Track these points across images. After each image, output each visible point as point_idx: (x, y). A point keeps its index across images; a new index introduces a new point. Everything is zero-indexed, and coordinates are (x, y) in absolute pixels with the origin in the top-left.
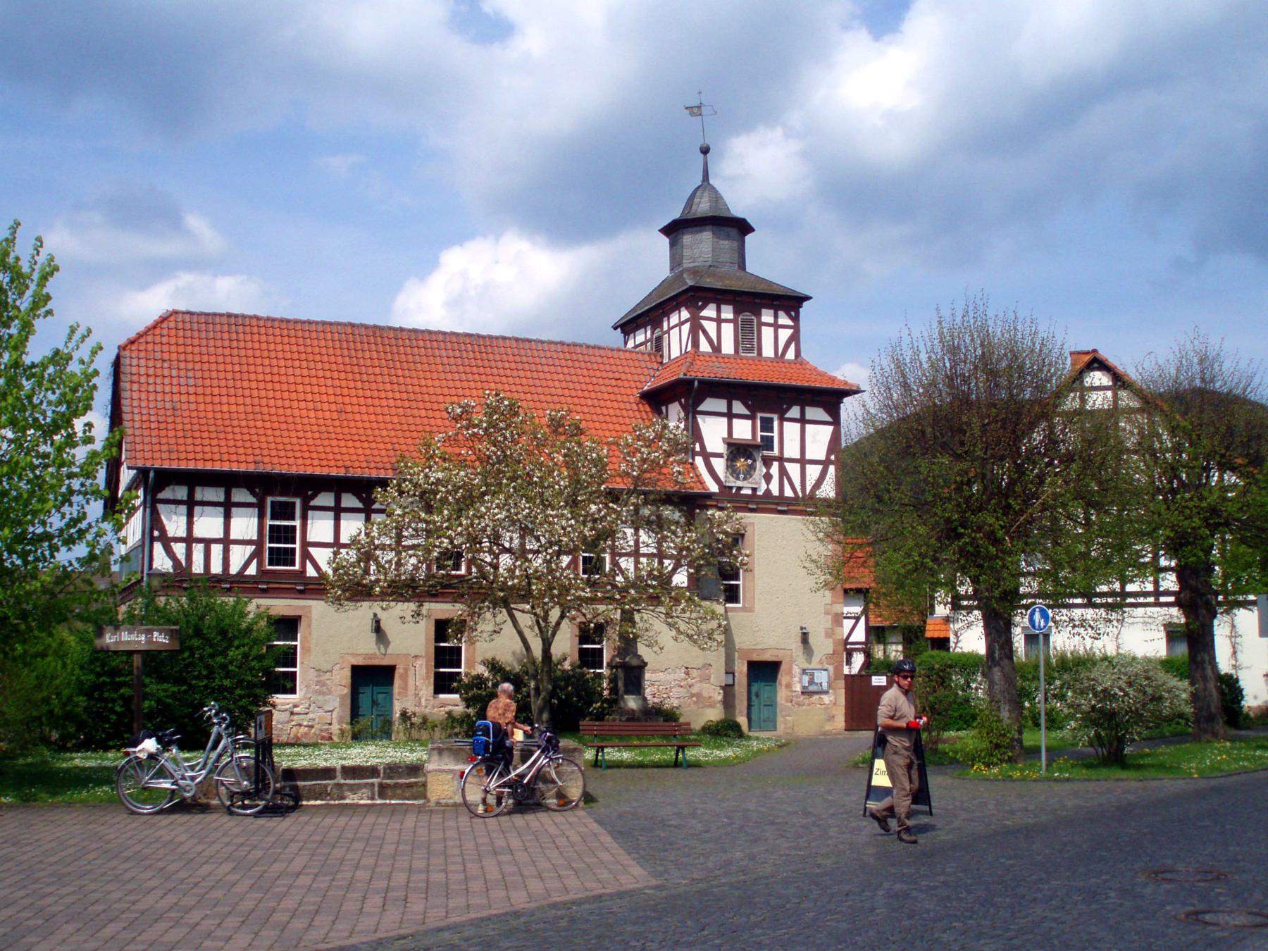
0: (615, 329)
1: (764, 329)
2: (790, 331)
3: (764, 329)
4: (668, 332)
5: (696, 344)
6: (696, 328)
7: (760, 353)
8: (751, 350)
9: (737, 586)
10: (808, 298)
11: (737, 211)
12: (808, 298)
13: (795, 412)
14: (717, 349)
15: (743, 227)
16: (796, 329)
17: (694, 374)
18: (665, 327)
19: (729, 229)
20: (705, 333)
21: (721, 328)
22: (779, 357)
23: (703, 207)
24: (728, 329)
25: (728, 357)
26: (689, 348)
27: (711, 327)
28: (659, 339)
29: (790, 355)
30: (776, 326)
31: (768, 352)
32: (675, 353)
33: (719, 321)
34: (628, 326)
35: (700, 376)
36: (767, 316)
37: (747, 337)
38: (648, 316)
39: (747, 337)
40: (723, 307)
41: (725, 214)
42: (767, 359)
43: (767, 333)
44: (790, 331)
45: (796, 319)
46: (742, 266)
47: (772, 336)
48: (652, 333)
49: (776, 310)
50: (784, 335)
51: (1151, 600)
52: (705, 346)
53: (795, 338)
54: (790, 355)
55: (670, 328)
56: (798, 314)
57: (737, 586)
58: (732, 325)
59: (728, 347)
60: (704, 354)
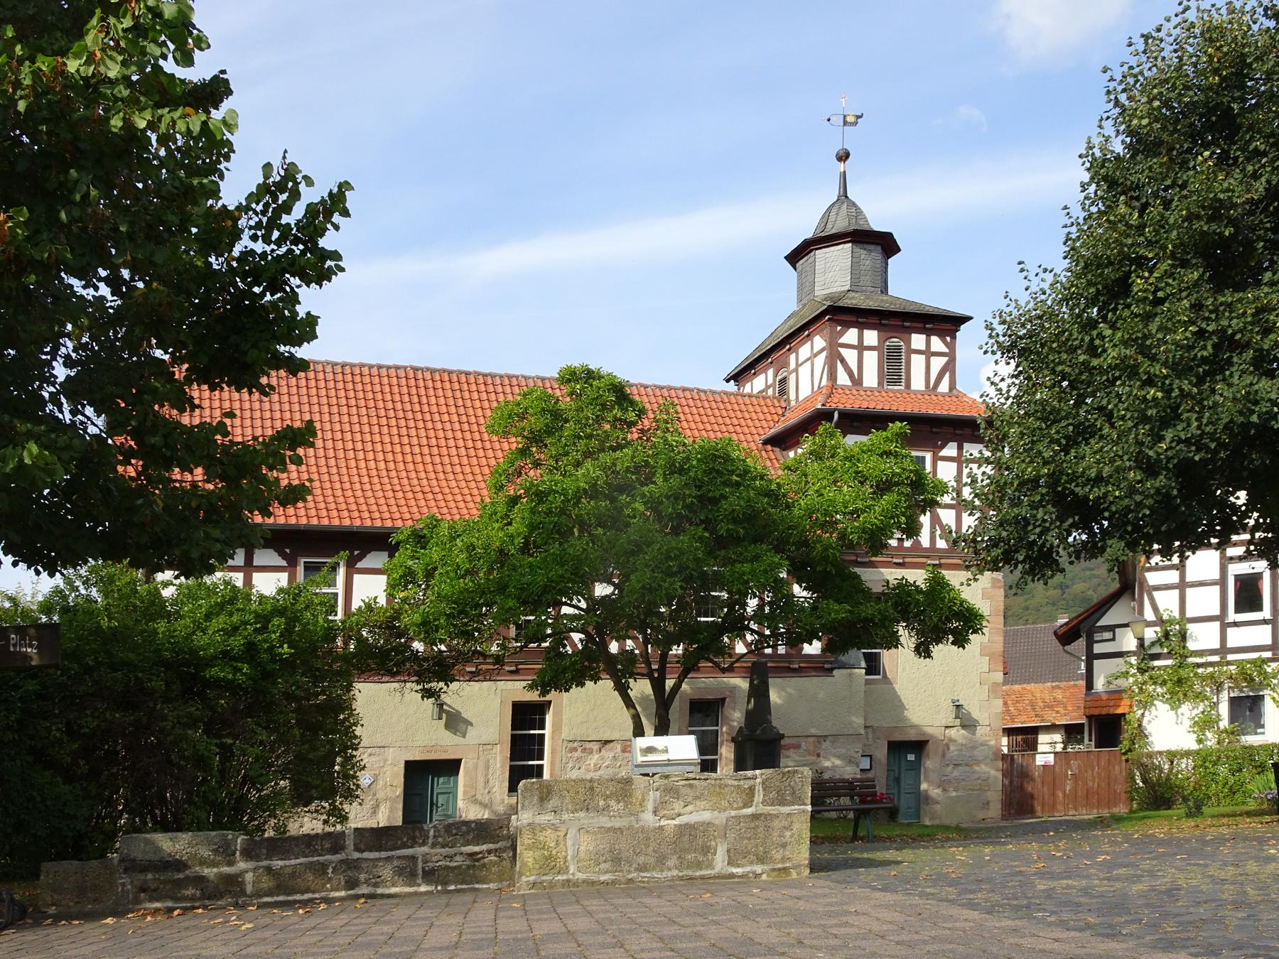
0: (728, 381)
1: (914, 356)
2: (944, 360)
3: (914, 356)
4: (796, 370)
5: (833, 376)
6: (834, 357)
7: (908, 386)
8: (897, 382)
9: (543, 735)
10: (971, 318)
11: (877, 226)
12: (971, 318)
13: (950, 450)
14: (857, 381)
15: (886, 245)
16: (951, 356)
17: (834, 406)
18: (793, 365)
19: (872, 247)
20: (843, 361)
21: (863, 352)
22: (932, 389)
23: (840, 224)
24: (871, 359)
25: (872, 390)
26: (824, 382)
27: (850, 356)
28: (784, 381)
29: (944, 387)
30: (928, 353)
31: (918, 383)
32: (805, 392)
33: (861, 348)
34: (739, 376)
35: (841, 407)
36: (918, 341)
37: (894, 368)
38: (773, 352)
39: (894, 368)
40: (866, 332)
41: (865, 228)
42: (916, 392)
43: (918, 362)
44: (944, 360)
45: (952, 347)
46: (885, 290)
47: (923, 359)
48: (776, 376)
49: (929, 333)
50: (937, 363)
51: (1216, 658)
52: (843, 379)
53: (950, 367)
54: (944, 387)
55: (798, 365)
56: (954, 338)
57: (543, 735)
58: (876, 353)
59: (871, 378)
60: (843, 387)
